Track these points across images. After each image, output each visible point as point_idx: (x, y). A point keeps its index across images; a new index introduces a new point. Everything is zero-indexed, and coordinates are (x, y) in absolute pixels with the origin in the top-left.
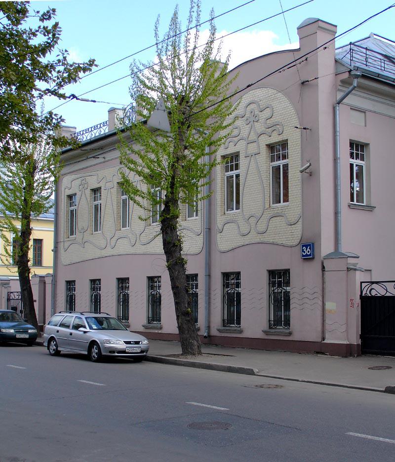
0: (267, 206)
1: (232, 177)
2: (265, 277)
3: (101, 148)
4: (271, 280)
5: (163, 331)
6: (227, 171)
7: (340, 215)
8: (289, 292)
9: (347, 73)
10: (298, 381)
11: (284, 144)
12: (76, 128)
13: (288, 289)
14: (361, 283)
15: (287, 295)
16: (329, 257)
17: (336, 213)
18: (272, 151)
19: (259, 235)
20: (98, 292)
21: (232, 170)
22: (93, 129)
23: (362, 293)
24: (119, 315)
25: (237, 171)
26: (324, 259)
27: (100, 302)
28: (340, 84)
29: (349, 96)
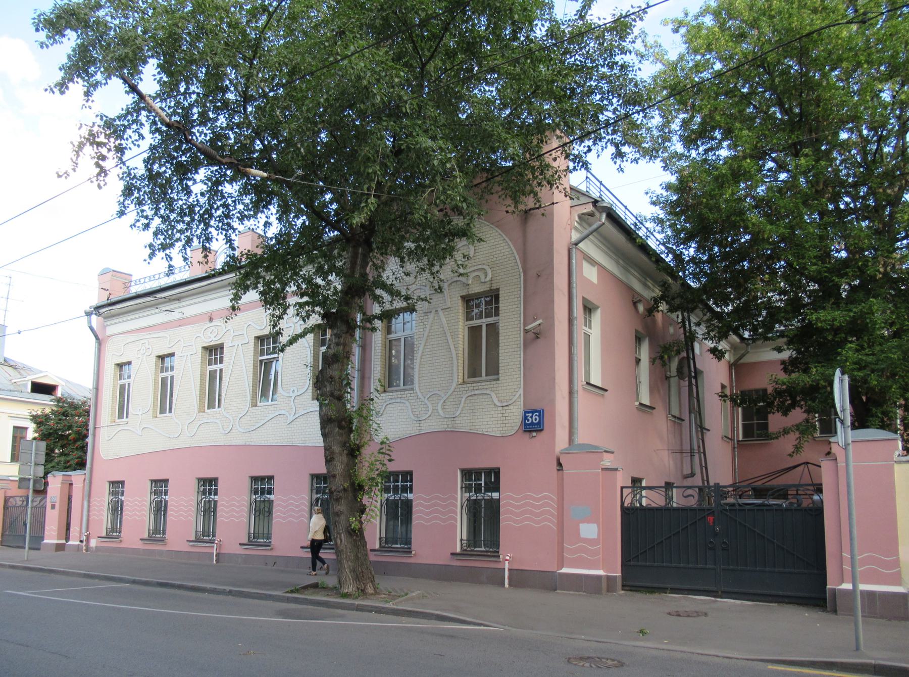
0: (461, 381)
1: (216, 371)
2: (248, 482)
3: (179, 299)
4: (315, 485)
5: (123, 545)
6: (210, 364)
7: (576, 395)
8: (411, 500)
9: (591, 205)
10: (134, 582)
11: (493, 297)
12: (131, 275)
13: (410, 496)
14: (622, 488)
15: (408, 505)
16: (565, 452)
17: (571, 393)
18: (262, 345)
19: (446, 420)
20: (120, 497)
21: (216, 363)
22: (147, 280)
23: (622, 503)
24: (158, 528)
25: (172, 373)
26: (561, 453)
27: (122, 510)
28: (577, 219)
29: (586, 240)
